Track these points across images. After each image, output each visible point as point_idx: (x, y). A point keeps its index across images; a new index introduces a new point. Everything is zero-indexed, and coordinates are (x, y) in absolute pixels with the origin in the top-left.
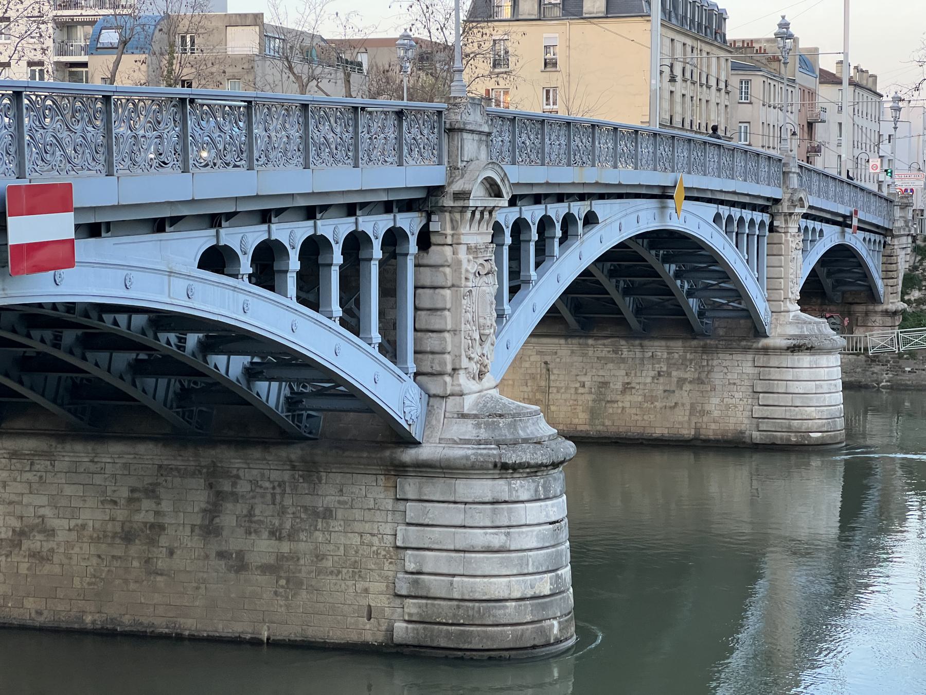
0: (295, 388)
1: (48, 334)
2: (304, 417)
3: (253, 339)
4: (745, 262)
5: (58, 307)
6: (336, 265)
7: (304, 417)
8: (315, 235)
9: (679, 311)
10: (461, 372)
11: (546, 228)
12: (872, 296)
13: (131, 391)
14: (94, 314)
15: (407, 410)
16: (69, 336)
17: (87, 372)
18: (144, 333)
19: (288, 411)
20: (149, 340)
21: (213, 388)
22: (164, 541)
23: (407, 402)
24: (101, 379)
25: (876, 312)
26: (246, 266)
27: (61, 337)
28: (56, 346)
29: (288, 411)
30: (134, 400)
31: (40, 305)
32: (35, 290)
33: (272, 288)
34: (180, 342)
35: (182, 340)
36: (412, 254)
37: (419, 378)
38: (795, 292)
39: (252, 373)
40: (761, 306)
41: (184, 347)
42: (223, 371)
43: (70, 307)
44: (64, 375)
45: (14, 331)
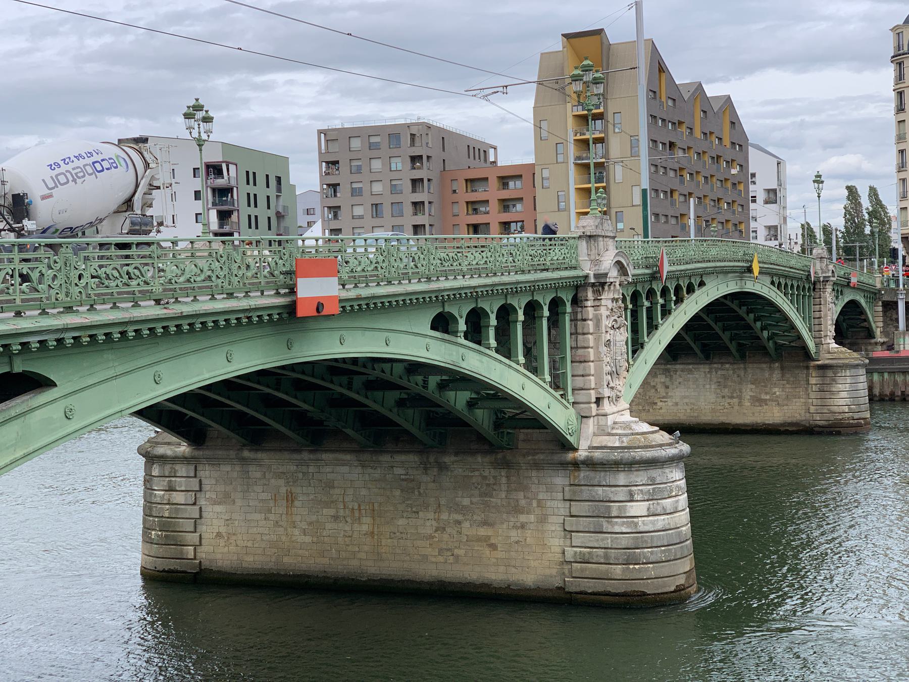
0: (499, 415)
1: (344, 379)
2: (505, 433)
3: (475, 382)
4: (795, 311)
5: (347, 361)
6: (461, 332)
7: (505, 433)
8: (506, 303)
9: (765, 348)
10: (606, 401)
11: (510, 314)
12: (870, 334)
13: (396, 418)
14: (369, 365)
15: (570, 427)
16: (358, 381)
17: (300, 407)
18: (401, 378)
19: (495, 430)
20: (404, 382)
21: (517, 417)
22: (434, 528)
23: (570, 423)
24: (379, 412)
25: (870, 343)
26: (462, 326)
27: (352, 383)
28: (350, 388)
29: (495, 430)
30: (398, 425)
31: (336, 360)
32: (308, 353)
33: (479, 343)
34: (424, 384)
35: (425, 382)
36: (568, 313)
37: (575, 405)
38: (831, 330)
39: (471, 404)
40: (811, 345)
41: (427, 387)
42: (452, 403)
43: (355, 361)
44: (287, 409)
45: (323, 379)
